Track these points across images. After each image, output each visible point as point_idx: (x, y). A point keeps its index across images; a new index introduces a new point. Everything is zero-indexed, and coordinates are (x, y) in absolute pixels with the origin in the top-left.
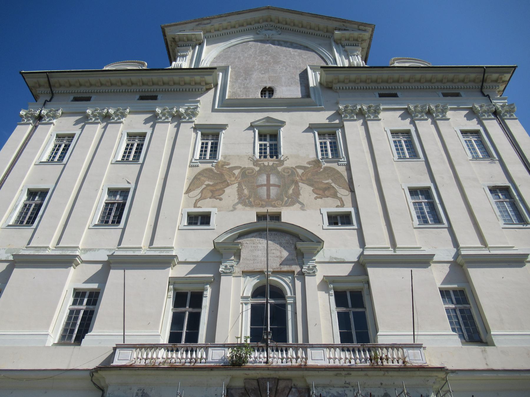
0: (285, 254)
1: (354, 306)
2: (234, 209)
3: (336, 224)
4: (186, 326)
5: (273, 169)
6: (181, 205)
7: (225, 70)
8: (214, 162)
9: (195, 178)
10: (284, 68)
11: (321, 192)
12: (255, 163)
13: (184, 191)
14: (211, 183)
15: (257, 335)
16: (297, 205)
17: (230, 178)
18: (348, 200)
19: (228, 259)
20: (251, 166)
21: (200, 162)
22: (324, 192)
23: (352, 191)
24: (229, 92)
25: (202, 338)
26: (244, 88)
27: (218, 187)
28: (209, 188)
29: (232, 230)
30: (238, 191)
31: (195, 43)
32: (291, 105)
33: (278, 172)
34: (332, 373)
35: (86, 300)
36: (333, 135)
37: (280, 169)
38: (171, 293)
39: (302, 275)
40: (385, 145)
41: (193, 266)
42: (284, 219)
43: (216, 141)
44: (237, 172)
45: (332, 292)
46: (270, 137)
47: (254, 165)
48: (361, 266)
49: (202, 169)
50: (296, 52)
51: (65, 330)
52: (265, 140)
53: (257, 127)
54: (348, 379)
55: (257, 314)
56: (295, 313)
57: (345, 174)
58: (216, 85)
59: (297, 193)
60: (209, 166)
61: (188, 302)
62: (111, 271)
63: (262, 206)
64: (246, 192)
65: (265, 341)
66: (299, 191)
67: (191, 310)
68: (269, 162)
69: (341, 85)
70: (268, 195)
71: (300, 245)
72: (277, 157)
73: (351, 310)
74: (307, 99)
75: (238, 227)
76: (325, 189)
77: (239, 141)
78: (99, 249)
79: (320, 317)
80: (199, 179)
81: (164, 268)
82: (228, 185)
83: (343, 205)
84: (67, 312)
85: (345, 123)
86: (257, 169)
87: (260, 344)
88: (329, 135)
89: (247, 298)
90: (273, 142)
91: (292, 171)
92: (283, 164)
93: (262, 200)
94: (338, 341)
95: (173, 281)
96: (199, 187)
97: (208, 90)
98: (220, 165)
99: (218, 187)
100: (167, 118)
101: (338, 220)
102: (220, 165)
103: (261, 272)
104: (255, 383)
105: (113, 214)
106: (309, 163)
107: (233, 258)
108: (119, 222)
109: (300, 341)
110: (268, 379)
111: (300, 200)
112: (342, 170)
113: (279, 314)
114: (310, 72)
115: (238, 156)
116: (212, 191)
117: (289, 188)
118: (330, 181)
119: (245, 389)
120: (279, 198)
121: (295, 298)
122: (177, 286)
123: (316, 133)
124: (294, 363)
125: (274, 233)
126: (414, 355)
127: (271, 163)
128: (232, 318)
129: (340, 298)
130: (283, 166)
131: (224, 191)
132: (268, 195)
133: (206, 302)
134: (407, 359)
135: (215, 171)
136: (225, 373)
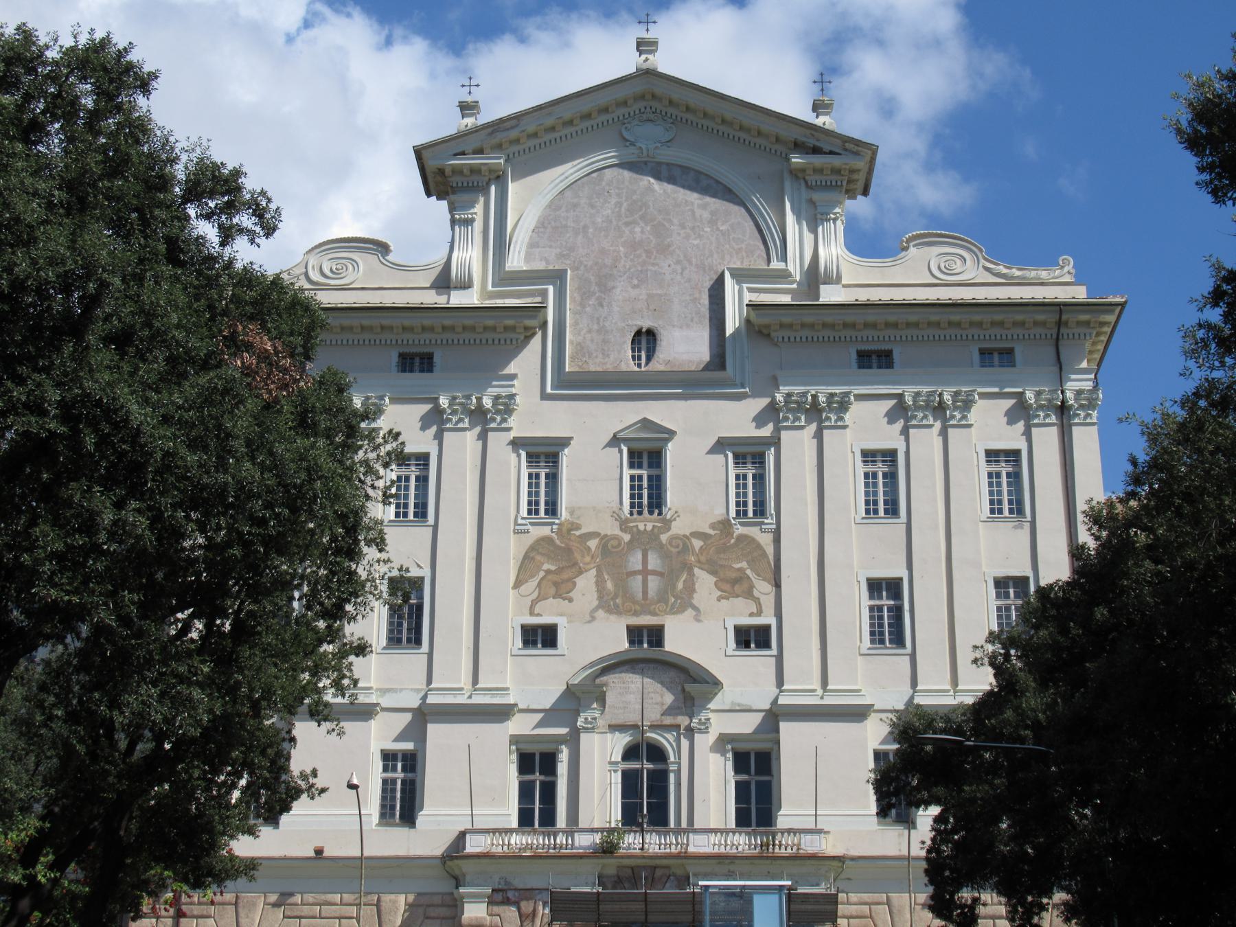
0: (669, 698)
1: (757, 773)
2: (593, 618)
3: (747, 646)
4: (538, 805)
5: (653, 536)
6: (509, 612)
7: (557, 277)
8: (553, 524)
9: (527, 557)
10: (679, 268)
11: (727, 587)
12: (624, 525)
13: (512, 584)
14: (553, 568)
15: (630, 816)
16: (690, 612)
17: (583, 556)
18: (768, 603)
19: (589, 707)
20: (617, 532)
21: (532, 524)
22: (734, 586)
23: (778, 585)
24: (571, 342)
25: (561, 820)
26: (599, 331)
27: (565, 576)
28: (550, 577)
29: (592, 664)
30: (597, 583)
31: (486, 179)
32: (689, 385)
33: (661, 546)
34: (714, 861)
35: (399, 765)
36: (759, 460)
37: (664, 538)
38: (514, 757)
39: (690, 732)
40: (849, 483)
41: (541, 715)
42: (668, 646)
43: (554, 471)
44: (593, 544)
45: (730, 755)
46: (647, 454)
47: (621, 530)
48: (774, 716)
49: (535, 538)
50: (704, 207)
51: (383, 806)
52: (640, 467)
53: (625, 440)
54: (732, 868)
55: (630, 782)
56: (678, 784)
57: (770, 550)
58: (544, 325)
59: (690, 589)
60: (546, 531)
61: (536, 764)
62: (429, 726)
63: (636, 614)
64: (609, 585)
65: (641, 825)
66: (694, 584)
67: (542, 778)
68: (646, 523)
69: (786, 333)
70: (645, 592)
71: (689, 687)
72: (660, 514)
73: (753, 779)
74: (716, 375)
75: (602, 660)
76: (735, 582)
77: (595, 484)
78: (401, 690)
79: (711, 789)
80: (533, 559)
81: (502, 721)
82: (580, 573)
83: (759, 613)
84: (380, 781)
85: (784, 435)
86: (627, 537)
87: (634, 828)
88: (750, 455)
89: (616, 763)
90: (654, 472)
91: (683, 543)
92: (669, 529)
93: (635, 602)
94: (732, 824)
95: (515, 740)
96: (532, 576)
97: (528, 338)
98: (564, 529)
99: (565, 576)
100: (461, 420)
101: (752, 638)
102: (564, 529)
103: (635, 727)
104: (630, 871)
105: (405, 625)
106: (713, 526)
107: (595, 705)
108: (418, 642)
109: (684, 825)
110: (644, 867)
111: (695, 602)
112: (766, 540)
113: (659, 782)
114: (729, 284)
115: (594, 508)
116: (556, 584)
117: (678, 578)
118: (744, 565)
119: (618, 877)
120: (662, 598)
121: (679, 764)
122: (522, 746)
123: (730, 455)
124: (673, 849)
125: (652, 666)
126: (812, 841)
127: (649, 527)
128: (596, 791)
129: (741, 762)
130: (670, 533)
131: (575, 584)
132: (645, 592)
133: (562, 768)
134: (802, 846)
135: (558, 542)
136: (596, 861)
